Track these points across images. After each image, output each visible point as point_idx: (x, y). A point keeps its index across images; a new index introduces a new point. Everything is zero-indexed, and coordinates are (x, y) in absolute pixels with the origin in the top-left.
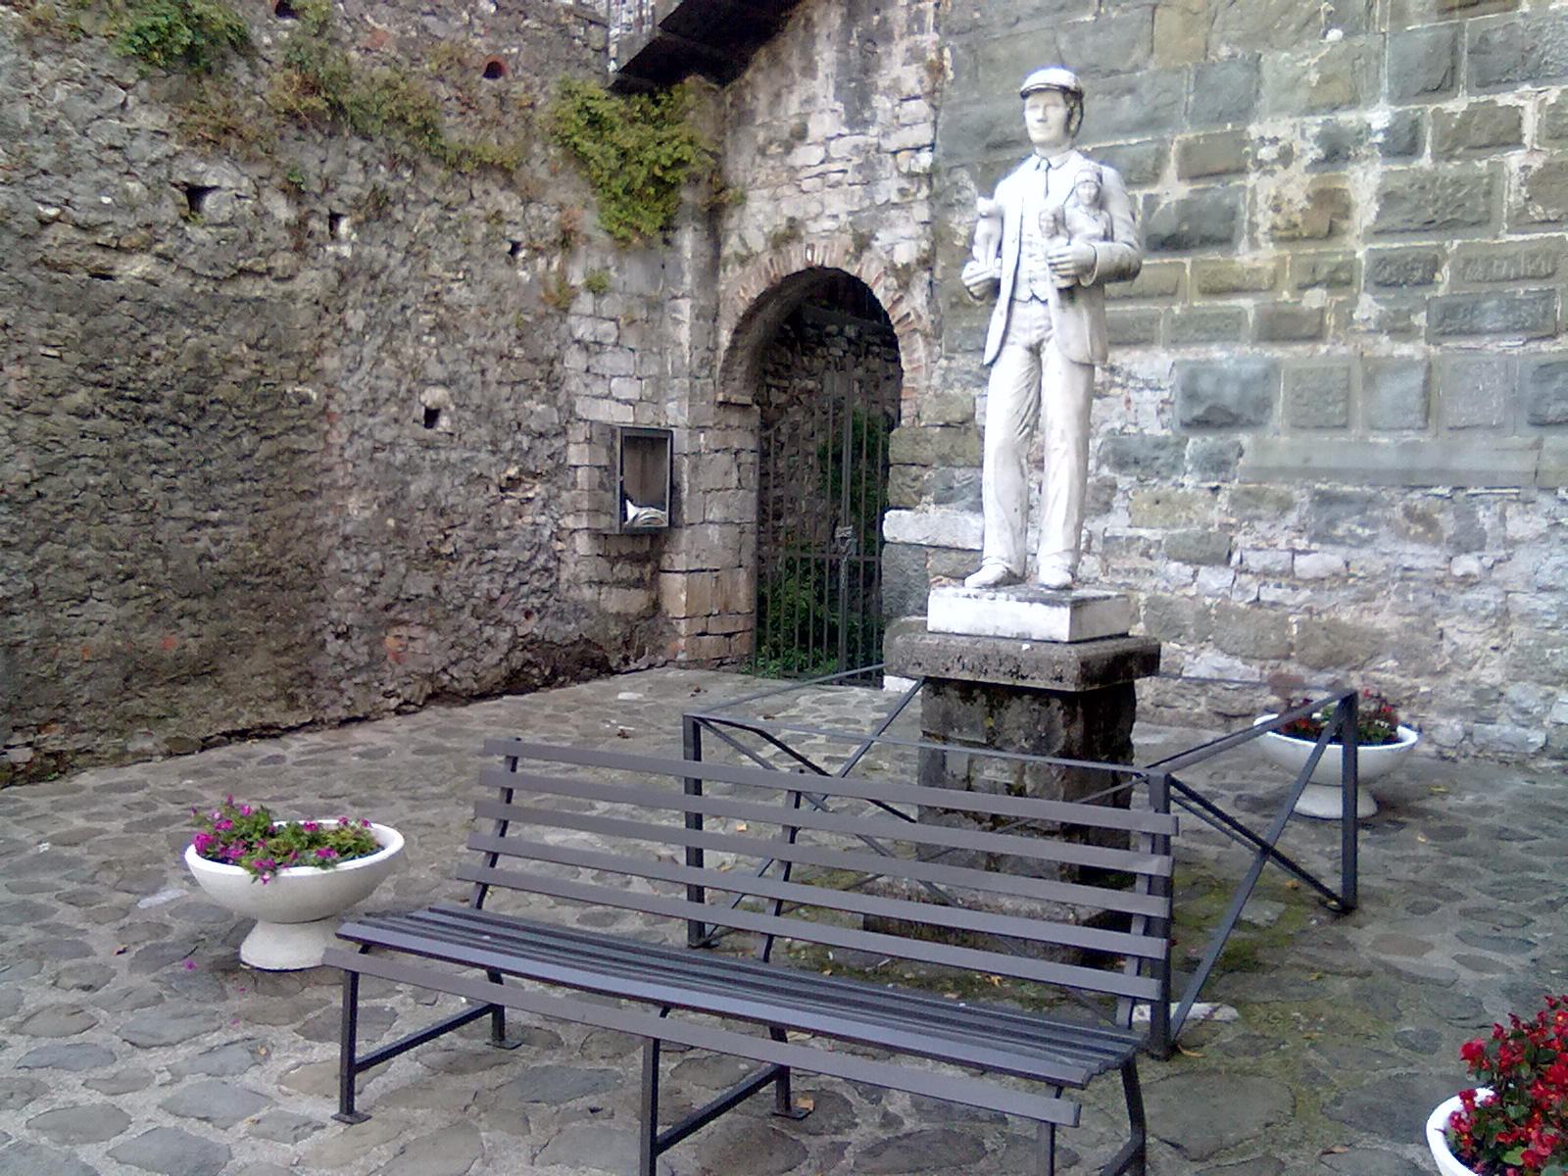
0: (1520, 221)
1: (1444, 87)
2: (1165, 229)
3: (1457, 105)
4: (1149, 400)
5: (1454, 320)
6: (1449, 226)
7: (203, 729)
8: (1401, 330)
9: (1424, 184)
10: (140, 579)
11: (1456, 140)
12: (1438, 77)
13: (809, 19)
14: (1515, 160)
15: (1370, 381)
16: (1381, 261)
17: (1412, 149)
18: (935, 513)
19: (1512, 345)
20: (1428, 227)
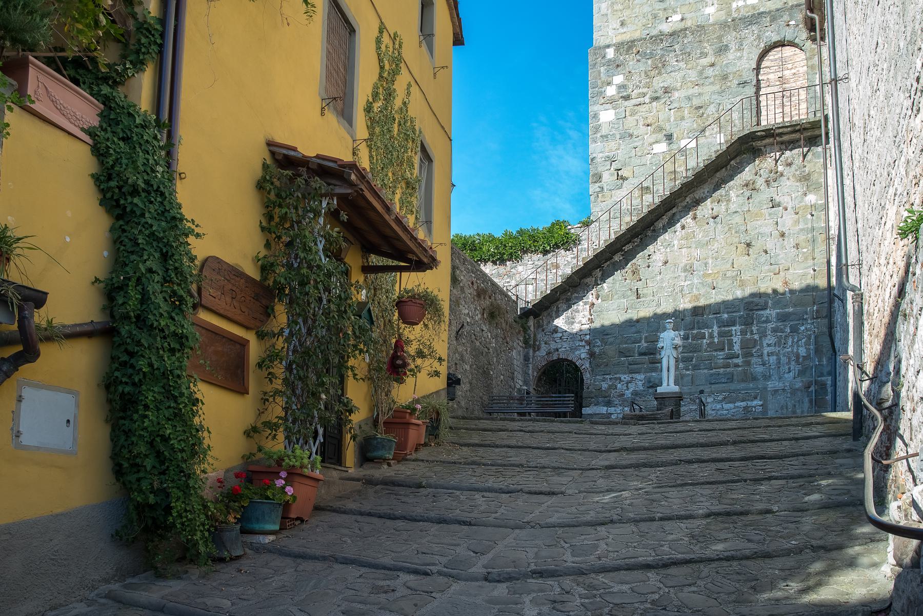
0: (706, 351)
1: (693, 329)
2: (643, 351)
3: (695, 332)
4: (640, 383)
5: (696, 367)
6: (695, 352)
7: (367, 507)
8: (688, 370)
9: (690, 344)
10: (160, 245)
11: (695, 338)
12: (774, 55)
13: (558, 308)
14: (705, 341)
15: (682, 378)
16: (683, 357)
17: (688, 339)
18: (595, 408)
19: (706, 371)
20: (691, 352)
